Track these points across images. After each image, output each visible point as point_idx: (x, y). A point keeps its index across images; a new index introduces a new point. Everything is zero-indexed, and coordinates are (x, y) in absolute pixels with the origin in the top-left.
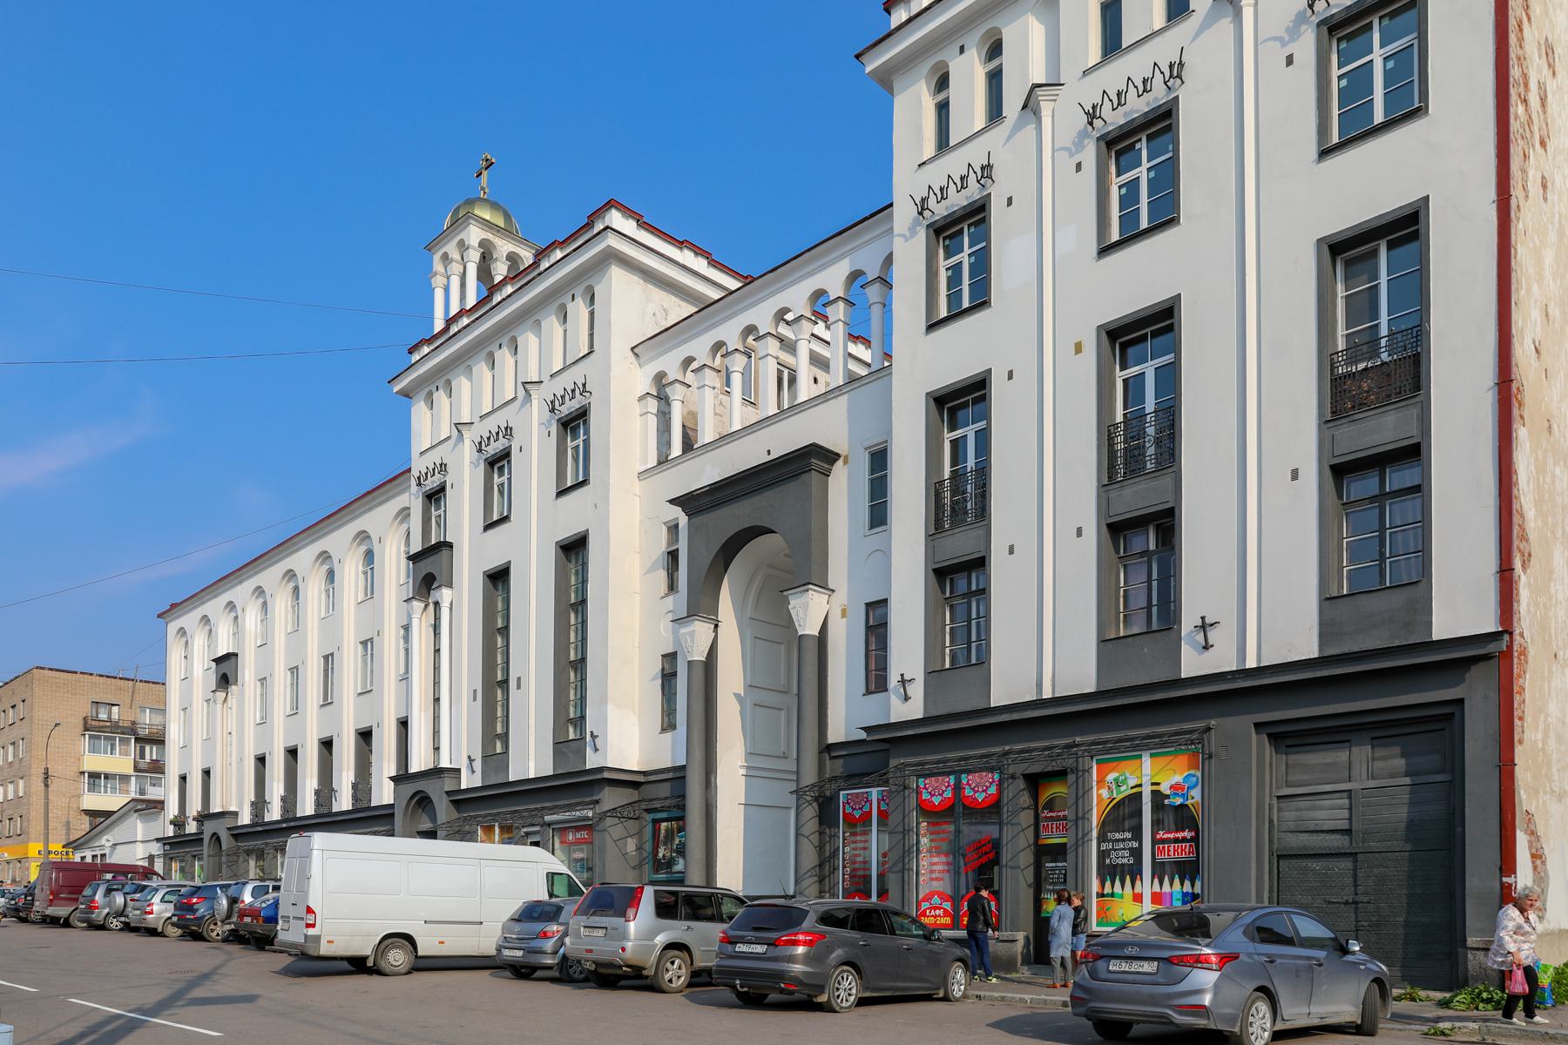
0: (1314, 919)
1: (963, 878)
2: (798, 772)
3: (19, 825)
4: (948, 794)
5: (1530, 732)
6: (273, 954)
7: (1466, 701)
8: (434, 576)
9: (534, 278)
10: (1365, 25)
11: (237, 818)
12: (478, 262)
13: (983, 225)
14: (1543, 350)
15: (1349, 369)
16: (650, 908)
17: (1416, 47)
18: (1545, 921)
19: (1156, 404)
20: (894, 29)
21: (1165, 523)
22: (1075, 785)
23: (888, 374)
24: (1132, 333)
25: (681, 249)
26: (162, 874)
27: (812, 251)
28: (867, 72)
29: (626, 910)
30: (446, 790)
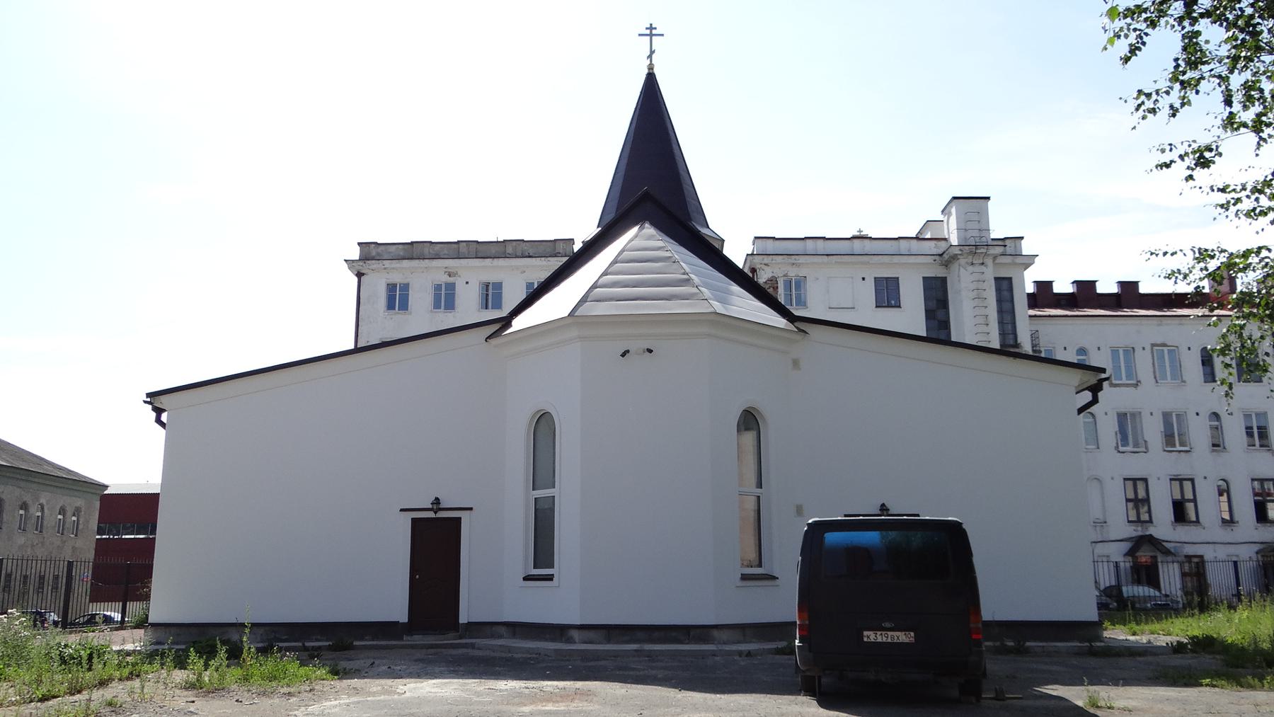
9: (51, 485)
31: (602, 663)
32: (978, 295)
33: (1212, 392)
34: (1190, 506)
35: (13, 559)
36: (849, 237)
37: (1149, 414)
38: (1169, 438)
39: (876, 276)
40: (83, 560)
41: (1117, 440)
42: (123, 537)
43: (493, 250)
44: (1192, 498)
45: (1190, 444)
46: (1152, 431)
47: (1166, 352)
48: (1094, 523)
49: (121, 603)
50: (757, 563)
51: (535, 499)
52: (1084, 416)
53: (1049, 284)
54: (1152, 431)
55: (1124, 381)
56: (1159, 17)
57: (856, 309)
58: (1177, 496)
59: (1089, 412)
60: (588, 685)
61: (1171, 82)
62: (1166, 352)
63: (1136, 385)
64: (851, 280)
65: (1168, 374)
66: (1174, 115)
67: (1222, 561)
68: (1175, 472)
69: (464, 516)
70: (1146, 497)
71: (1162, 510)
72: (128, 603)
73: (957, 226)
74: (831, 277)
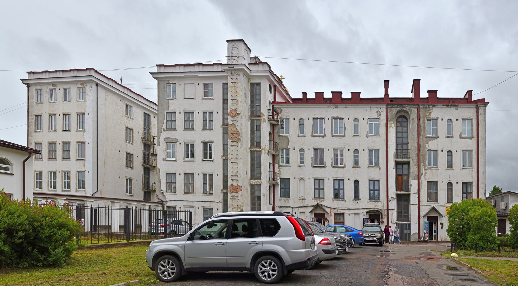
0: (132, 157)
1: (348, 106)
2: (171, 129)
3: (208, 153)
4: (189, 226)
5: (388, 249)
6: (34, 186)
7: (261, 84)
8: (306, 92)
9: (49, 178)
10: (154, 112)
11: (227, 85)
12: (90, 84)
13: (272, 210)
14: (357, 216)
15: (173, 220)
16: (368, 155)
17: (210, 143)
18: (293, 147)
19: (34, 198)
20: (418, 174)
21: (252, 145)
22: (120, 83)
23: (144, 243)
24: (220, 274)
25: (109, 80)
26: (157, 104)
27: (66, 76)
28: (235, 223)
29: (360, 98)
30: (251, 56)
31: (129, 189)
32: (236, 189)
33: (450, 176)
34: (341, 192)
35: (188, 212)
36: (359, 230)
37: (181, 174)
38: (315, 159)
39: (380, 151)
40: (187, 211)
41: (313, 130)
42: (501, 234)
43: (225, 164)
44: (320, 197)
45: (325, 164)
46: (328, 158)
47: (467, 166)
48: (300, 198)
49: (97, 224)
50: (427, 100)
51: (194, 174)
52: (416, 147)
53: (436, 92)
54: (328, 158)
55: (319, 134)
56: (484, 206)
57: (213, 130)
58: (337, 187)
59: (101, 195)
60: (375, 248)
61: (383, 221)
62: (171, 97)
63: (323, 137)
64: (399, 145)
65: (400, 160)
66: (380, 168)
67: (182, 212)
68: (336, 176)
69: (183, 194)
70: (463, 194)
71: (329, 192)
72: (123, 224)
73: (264, 241)
74: (52, 93)
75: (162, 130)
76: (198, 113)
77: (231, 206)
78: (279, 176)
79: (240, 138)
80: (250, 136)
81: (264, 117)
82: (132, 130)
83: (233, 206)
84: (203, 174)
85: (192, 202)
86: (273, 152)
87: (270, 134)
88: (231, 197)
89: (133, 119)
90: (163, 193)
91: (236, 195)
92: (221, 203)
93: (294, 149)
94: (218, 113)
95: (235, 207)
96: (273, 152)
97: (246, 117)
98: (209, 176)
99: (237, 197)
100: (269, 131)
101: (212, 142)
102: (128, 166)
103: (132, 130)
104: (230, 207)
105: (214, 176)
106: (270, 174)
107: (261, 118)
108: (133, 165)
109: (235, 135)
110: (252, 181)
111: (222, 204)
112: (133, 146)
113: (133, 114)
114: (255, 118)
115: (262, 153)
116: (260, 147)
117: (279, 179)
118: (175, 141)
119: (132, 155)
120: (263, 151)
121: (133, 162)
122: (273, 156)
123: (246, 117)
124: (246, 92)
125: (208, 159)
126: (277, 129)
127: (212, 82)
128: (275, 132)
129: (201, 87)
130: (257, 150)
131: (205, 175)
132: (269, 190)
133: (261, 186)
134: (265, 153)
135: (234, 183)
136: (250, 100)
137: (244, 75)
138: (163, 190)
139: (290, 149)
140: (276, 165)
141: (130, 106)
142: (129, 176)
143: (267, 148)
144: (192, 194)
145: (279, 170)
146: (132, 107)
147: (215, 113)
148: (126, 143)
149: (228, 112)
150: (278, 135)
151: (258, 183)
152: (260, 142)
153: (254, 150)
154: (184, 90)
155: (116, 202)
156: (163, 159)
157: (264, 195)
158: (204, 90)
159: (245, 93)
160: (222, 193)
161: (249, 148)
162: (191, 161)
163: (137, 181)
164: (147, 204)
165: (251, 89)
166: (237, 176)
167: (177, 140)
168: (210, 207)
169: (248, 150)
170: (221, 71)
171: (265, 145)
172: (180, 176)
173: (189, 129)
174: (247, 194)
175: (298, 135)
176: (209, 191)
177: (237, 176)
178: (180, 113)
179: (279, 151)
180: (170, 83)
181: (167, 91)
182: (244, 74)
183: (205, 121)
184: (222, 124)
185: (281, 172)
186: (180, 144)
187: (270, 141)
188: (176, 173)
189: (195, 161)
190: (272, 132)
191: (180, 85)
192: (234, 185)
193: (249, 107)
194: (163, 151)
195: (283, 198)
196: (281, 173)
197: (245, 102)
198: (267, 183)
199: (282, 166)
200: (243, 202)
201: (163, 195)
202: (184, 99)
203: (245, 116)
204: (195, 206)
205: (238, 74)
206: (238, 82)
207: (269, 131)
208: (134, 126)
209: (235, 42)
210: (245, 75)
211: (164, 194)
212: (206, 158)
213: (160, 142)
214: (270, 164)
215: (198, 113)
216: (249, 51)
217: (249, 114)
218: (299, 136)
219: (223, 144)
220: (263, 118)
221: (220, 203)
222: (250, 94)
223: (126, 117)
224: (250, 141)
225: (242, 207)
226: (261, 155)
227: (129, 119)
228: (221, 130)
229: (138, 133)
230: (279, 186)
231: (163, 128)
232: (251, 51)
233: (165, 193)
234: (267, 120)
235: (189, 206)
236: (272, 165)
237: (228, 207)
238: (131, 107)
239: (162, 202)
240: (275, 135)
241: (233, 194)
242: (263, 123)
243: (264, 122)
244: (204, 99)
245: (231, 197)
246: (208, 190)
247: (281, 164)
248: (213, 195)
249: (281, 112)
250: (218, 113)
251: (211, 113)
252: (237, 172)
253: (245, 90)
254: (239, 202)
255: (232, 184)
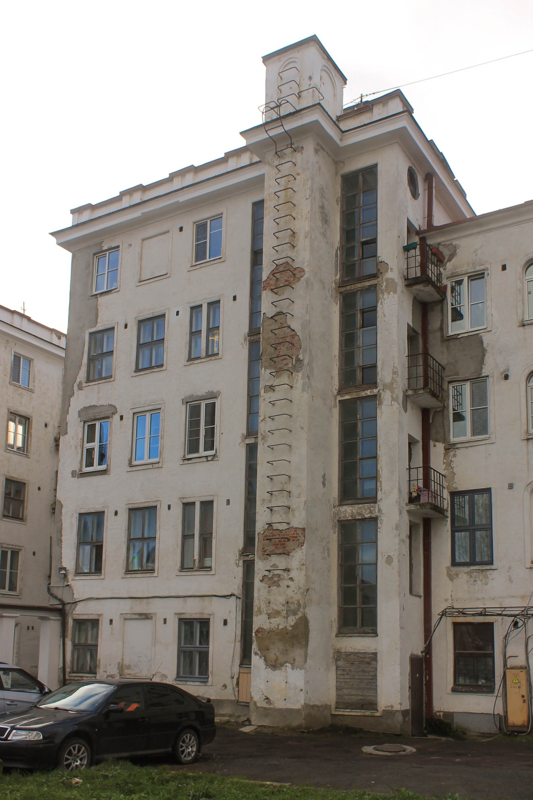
18: (502, 370)
69: (123, 575)
73: (423, 477)
75: (76, 388)
76: (178, 313)
77: (263, 606)
78: (445, 484)
79: (301, 357)
80: (341, 350)
81: (389, 275)
82: (29, 419)
83: (271, 605)
84: (183, 503)
85: (145, 600)
86: (428, 401)
87: (412, 337)
88: (266, 573)
89: (32, 391)
90: (65, 576)
91: (282, 566)
92: (237, 597)
93: (506, 377)
94: (235, 298)
95: (279, 608)
96: (428, 401)
97: (324, 288)
98: (201, 508)
99: (287, 570)
100: (408, 324)
101: (214, 396)
102: (11, 515)
103: (29, 419)
104: (260, 612)
105: (219, 509)
106: (414, 477)
107: (379, 279)
108: (25, 514)
109: (283, 350)
110: (343, 509)
111: (240, 602)
112: (29, 460)
113: (34, 378)
114: (359, 285)
115: (381, 403)
116: (374, 384)
117: (446, 494)
118: (108, 413)
119: (25, 484)
120: (386, 396)
121: (25, 504)
122: (425, 413)
123: (324, 288)
124: (326, 203)
125: (202, 452)
126: (440, 318)
127: (219, 212)
128: (430, 327)
129: (190, 232)
130: (363, 394)
131: (188, 506)
132: (410, 537)
133: (379, 525)
134: (393, 399)
135: (276, 518)
136: (342, 229)
137: (319, 148)
138: (65, 569)
139: (490, 380)
140: (435, 446)
141: (25, 358)
142: (12, 543)
143: (402, 382)
144: (148, 575)
145: (449, 465)
146: (32, 360)
147: (226, 306)
148: (8, 455)
149: (264, 278)
150: (442, 336)
151: (367, 516)
152: (374, 366)
153: (354, 395)
154: (141, 258)
155: (51, 618)
156: (74, 474)
157: (389, 560)
158: (197, 240)
159: (322, 207)
160: (241, 563)
161: (336, 392)
162: (151, 466)
163: (34, 554)
164: (4, 614)
165: (343, 196)
166: (290, 492)
167: (115, 407)
168: (202, 614)
169: (333, 399)
170: (251, 164)
171: (394, 373)
172: (40, 492)
173: (151, 368)
174: (324, 558)
175: (523, 321)
176: (200, 561)
177: (290, 492)
178: (126, 326)
179: (448, 391)
180: (104, 248)
181: (95, 275)
182: (318, 144)
183: (194, 334)
184: (246, 330)
185: (455, 471)
186: (122, 418)
187: (412, 356)
188: (106, 511)
189: (160, 465)
190: (419, 330)
191: (130, 245)
192: (275, 526)
193: (337, 254)
194: (73, 447)
195: (466, 569)
196: (455, 474)
197: (324, 235)
198: (400, 513)
199: (458, 446)
200: (308, 590)
201: (66, 584)
202: (140, 282)
203: (322, 282)
204: (155, 614)
205: (298, 147)
206: (298, 174)
207: (408, 324)
208: (33, 408)
209: (289, 52)
210: (323, 149)
211: (68, 581)
212: (197, 450)
213: (67, 424)
214: (412, 442)
215: (178, 313)
216: (338, 80)
217: (338, 277)
218: (524, 325)
219: (248, 394)
220: (387, 280)
221: (233, 598)
222: (343, 213)
223: (12, 387)
224: (340, 369)
225: (305, 607)
226: (378, 410)
227: (21, 391)
228: (244, 353)
229: (46, 425)
230: (449, 520)
231: (78, 380)
232: (345, 80)
233: (70, 577)
234: (400, 284)
235: (136, 617)
236: (420, 445)
237: (255, 609)
238: (30, 361)
239: (60, 607)
240: (431, 337)
241: (275, 560)
242: (386, 296)
243: (389, 293)
244: (195, 268)
245: (266, 573)
246: (196, 557)
247: (453, 440)
248: (213, 572)
249: (452, 255)
250: (235, 298)
251: (214, 305)
252: (290, 477)
253: (322, 196)
254: (292, 589)
255: (270, 525)
